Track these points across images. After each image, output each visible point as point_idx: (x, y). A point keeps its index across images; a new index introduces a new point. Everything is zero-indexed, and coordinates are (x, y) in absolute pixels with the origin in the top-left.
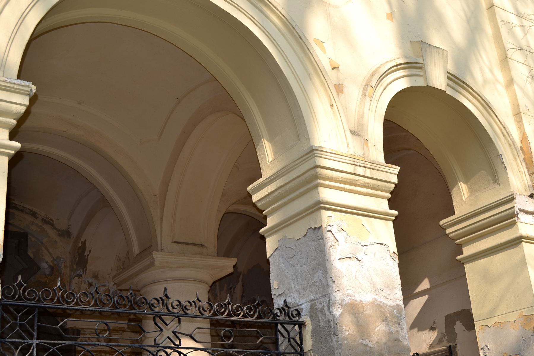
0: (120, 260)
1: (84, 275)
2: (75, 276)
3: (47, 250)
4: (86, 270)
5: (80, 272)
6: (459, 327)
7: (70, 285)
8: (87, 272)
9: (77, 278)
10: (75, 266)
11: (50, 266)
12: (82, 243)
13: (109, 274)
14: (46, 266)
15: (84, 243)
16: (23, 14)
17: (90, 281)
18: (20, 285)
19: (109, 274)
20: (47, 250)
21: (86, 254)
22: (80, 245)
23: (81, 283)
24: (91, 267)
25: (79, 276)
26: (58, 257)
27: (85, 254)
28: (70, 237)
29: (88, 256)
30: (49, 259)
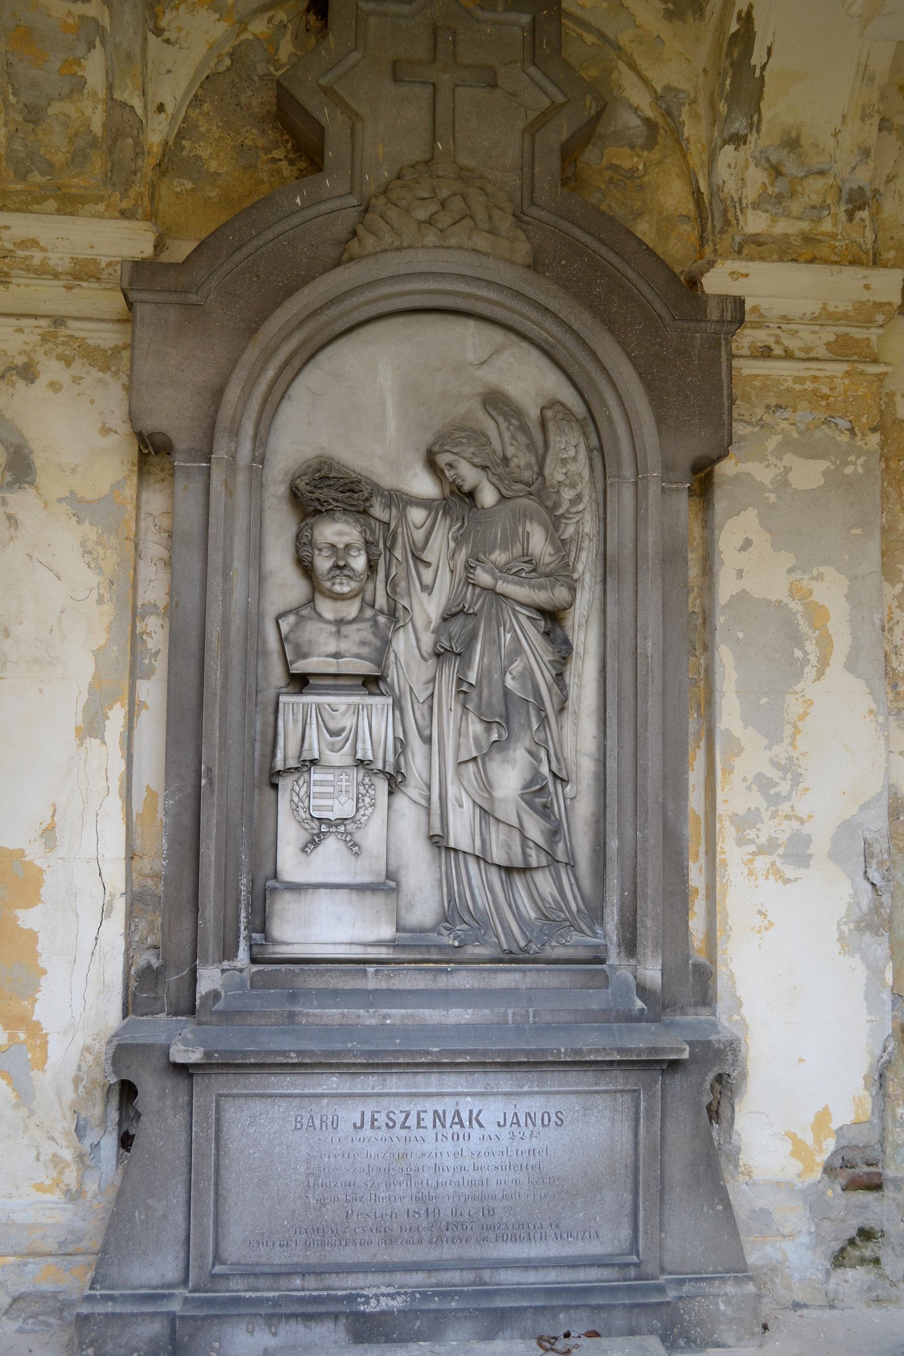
0: (871, 79)
1: (752, 138)
2: (726, 142)
3: (633, 67)
4: (760, 121)
5: (739, 125)
6: (502, 1123)
7: (710, 173)
8: (764, 127)
9: (729, 148)
10: (723, 107)
11: (647, 120)
12: (739, 18)
13: (835, 135)
14: (635, 122)
15: (747, 19)
16: (613, 384)
17: (774, 159)
18: (708, 1306)
19: (835, 135)
20: (633, 67)
21: (757, 58)
22: (734, 27)
23: (747, 167)
24: (777, 110)
25: (738, 140)
26: (668, 88)
27: (753, 61)
28: (702, 16)
29: (763, 68)
30: (639, 97)
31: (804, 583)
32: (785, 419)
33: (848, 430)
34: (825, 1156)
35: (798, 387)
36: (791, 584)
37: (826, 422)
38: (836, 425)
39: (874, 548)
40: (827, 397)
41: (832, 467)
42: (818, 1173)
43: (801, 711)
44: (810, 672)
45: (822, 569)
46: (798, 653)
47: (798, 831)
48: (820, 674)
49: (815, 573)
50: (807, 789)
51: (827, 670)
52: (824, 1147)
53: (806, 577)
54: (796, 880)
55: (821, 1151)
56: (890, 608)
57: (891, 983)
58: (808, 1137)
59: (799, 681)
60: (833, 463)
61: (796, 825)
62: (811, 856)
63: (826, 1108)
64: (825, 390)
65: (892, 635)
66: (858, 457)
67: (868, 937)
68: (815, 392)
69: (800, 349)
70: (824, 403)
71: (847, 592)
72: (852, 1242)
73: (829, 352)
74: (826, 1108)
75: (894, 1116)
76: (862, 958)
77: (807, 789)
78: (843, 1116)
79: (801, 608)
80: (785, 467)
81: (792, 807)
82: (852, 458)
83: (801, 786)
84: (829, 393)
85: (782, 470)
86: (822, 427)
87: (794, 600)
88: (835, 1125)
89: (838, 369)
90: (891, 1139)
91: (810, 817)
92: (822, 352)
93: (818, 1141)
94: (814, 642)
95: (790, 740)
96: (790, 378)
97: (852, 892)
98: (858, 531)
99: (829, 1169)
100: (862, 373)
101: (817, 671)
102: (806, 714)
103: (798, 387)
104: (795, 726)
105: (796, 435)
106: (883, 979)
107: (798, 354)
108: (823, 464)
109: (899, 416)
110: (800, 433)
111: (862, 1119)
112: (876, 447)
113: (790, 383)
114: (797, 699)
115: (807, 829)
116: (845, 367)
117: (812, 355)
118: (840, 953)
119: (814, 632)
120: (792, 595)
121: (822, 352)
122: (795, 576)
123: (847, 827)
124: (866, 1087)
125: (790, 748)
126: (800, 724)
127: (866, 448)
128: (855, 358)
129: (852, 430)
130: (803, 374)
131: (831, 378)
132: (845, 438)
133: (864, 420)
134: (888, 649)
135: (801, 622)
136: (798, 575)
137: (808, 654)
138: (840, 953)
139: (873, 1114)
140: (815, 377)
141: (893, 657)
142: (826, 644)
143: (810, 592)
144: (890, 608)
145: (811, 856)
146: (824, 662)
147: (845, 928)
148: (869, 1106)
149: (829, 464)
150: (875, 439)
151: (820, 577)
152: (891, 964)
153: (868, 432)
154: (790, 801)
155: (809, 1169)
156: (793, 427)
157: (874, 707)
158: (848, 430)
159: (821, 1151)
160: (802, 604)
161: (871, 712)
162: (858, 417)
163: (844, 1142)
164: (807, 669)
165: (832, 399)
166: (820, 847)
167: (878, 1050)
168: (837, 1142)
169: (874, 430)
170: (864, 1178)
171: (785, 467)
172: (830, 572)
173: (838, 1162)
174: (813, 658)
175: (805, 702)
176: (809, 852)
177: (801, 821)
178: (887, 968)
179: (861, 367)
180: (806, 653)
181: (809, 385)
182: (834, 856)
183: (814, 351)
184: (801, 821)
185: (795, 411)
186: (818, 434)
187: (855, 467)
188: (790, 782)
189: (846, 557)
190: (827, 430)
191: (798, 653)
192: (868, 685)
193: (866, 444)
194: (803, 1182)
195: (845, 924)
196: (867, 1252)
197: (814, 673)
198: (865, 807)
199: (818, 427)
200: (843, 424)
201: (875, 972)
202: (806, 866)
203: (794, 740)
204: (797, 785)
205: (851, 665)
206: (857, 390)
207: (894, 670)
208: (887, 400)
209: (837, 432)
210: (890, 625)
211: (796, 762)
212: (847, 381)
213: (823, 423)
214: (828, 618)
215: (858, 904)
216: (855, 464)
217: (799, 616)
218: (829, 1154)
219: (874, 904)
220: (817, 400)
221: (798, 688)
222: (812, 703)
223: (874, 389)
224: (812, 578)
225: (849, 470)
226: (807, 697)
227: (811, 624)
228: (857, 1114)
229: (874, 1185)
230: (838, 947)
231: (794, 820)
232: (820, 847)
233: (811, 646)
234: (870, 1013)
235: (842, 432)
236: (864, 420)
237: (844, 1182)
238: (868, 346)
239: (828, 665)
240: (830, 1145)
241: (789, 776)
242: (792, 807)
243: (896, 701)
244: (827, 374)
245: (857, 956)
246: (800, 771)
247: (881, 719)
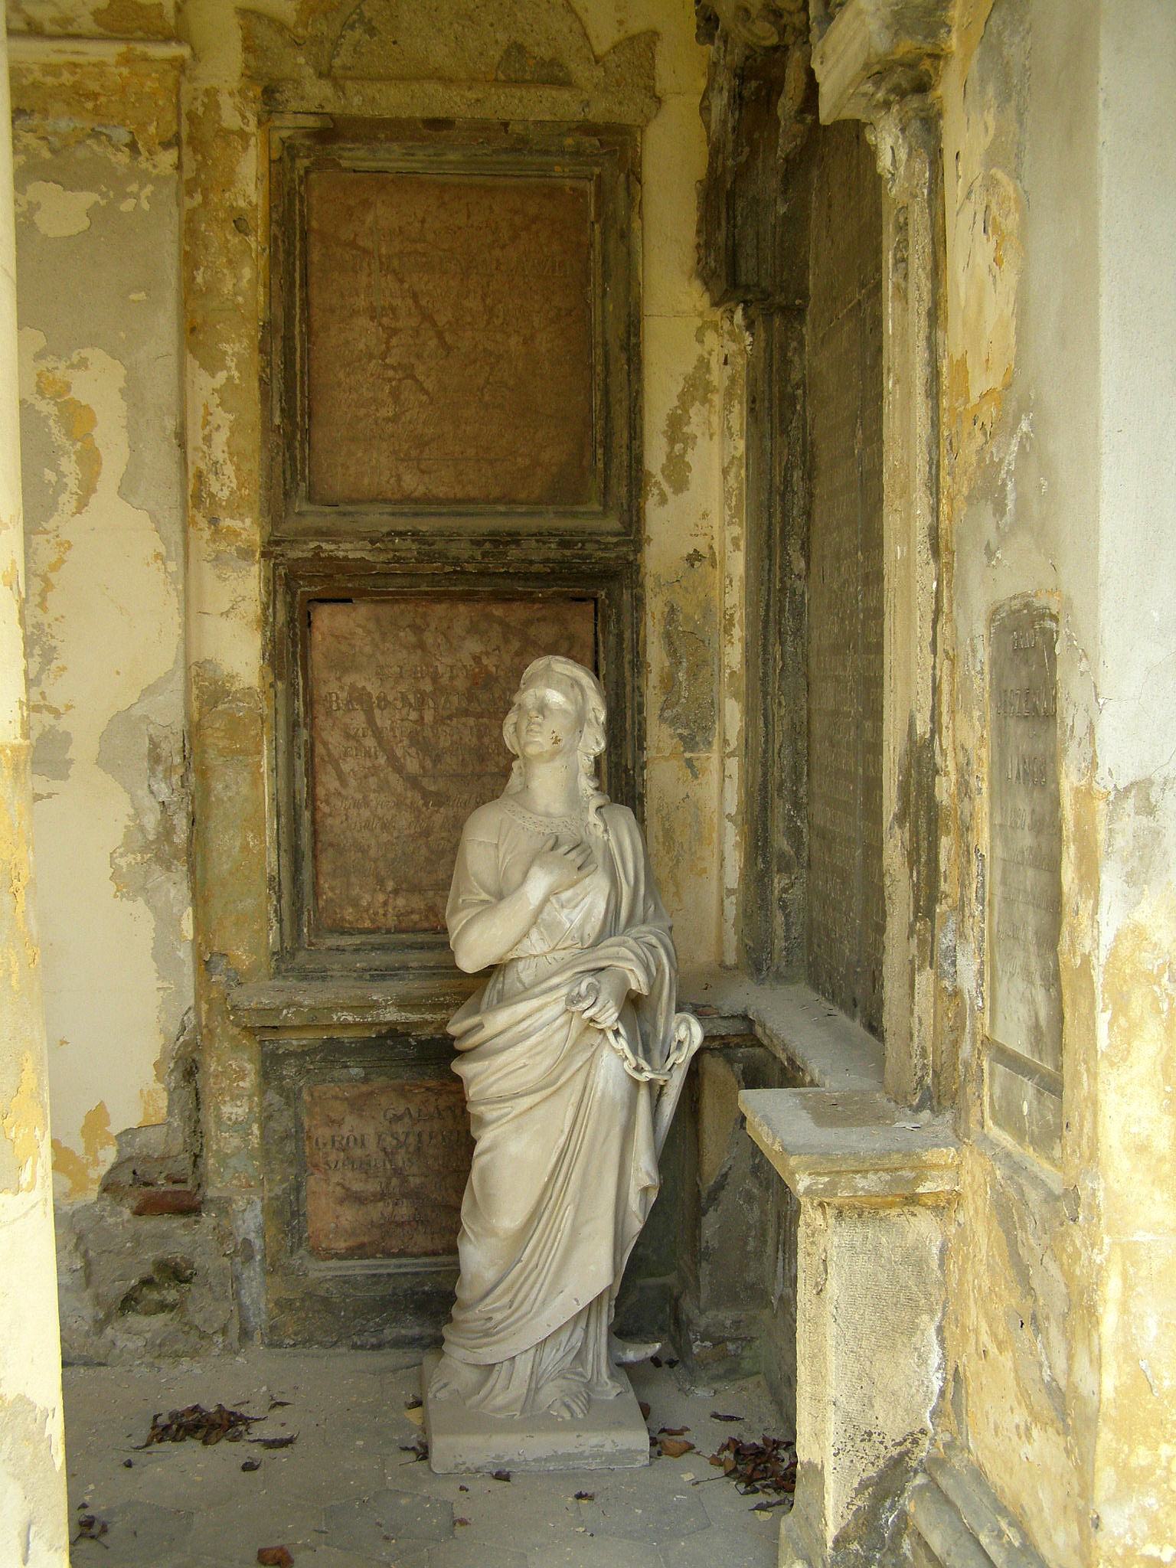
31: (58, 374)
32: (31, 131)
33: (126, 145)
34: (103, 1170)
35: (50, 80)
36: (39, 375)
37: (95, 134)
38: (109, 138)
39: (165, 324)
40: (95, 96)
41: (103, 203)
42: (93, 1194)
43: (54, 559)
44: (67, 502)
45: (86, 352)
46: (50, 475)
47: (52, 727)
48: (82, 504)
49: (75, 358)
50: (64, 669)
51: (93, 500)
52: (101, 1158)
53: (62, 365)
54: (49, 796)
55: (97, 1162)
56: (206, 407)
57: (190, 936)
58: (77, 1145)
59: (52, 515)
60: (103, 195)
61: (48, 718)
62: (71, 762)
63: (102, 1105)
64: (93, 86)
65: (210, 447)
66: (142, 187)
67: (158, 874)
68: (76, 88)
69: (54, 21)
70: (90, 105)
71: (122, 384)
72: (147, 1282)
73: (99, 25)
74: (102, 1105)
75: (219, 1117)
76: (147, 902)
77: (64, 669)
78: (126, 1115)
79: (54, 410)
80: (29, 203)
81: (43, 694)
82: (133, 188)
83: (53, 666)
84: (98, 89)
85: (25, 207)
86: (88, 142)
87: (44, 398)
88: (115, 1128)
89: (108, 52)
90: (215, 1147)
91: (69, 707)
92: (87, 24)
93: (90, 1148)
94: (74, 458)
95: (38, 599)
96: (36, 67)
97: (132, 812)
98: (141, 296)
99: (109, 1187)
100: (145, 59)
101: (79, 501)
102: (62, 561)
103: (50, 80)
104: (45, 579)
105: (47, 155)
106: (179, 932)
107: (49, 28)
108: (88, 198)
109: (224, 125)
110: (53, 151)
111: (154, 1121)
112: (170, 171)
113: (38, 75)
114: (48, 541)
115: (63, 725)
116: (121, 48)
117: (71, 30)
118: (115, 896)
119: (73, 445)
120: (41, 392)
121: (87, 24)
122: (43, 365)
123: (123, 721)
124: (159, 1078)
125: (39, 611)
126: (53, 577)
127: (155, 172)
128: (140, 34)
129: (133, 146)
130: (56, 59)
131: (100, 65)
132: (123, 158)
133: (152, 129)
134: (203, 467)
135: (55, 431)
136: (49, 362)
137: (65, 476)
138: (115, 896)
139: (170, 1113)
140: (75, 65)
141: (212, 477)
142: (90, 460)
143: (68, 387)
144: (206, 407)
145: (71, 762)
146: (88, 488)
147: (122, 862)
148: (163, 1102)
149: (99, 198)
150: (169, 157)
151: (83, 364)
152: (190, 910)
153: (159, 148)
154: (38, 685)
155: (80, 1187)
156: (42, 143)
157: (162, 550)
158: (126, 145)
159: (97, 1162)
160: (56, 404)
161: (158, 556)
162: (143, 126)
163: (129, 1151)
164: (64, 498)
165: (103, 99)
166: (84, 748)
167: (174, 1029)
168: (118, 1151)
169: (166, 145)
170: (169, 1198)
171: (29, 203)
172: (96, 356)
173: (126, 1178)
174: (72, 483)
175: (60, 544)
176: (68, 756)
177: (57, 713)
178: (185, 915)
179: (140, 48)
180: (61, 475)
181: (67, 78)
182: (106, 761)
183: (75, 25)
184: (57, 713)
185: (46, 117)
186: (81, 153)
187: (138, 200)
188: (38, 659)
189: (122, 335)
190: (95, 147)
191: (50, 475)
192: (153, 516)
193: (155, 166)
194: (72, 1204)
195: (122, 855)
196: (171, 1295)
197: (74, 503)
198: (149, 691)
199: (79, 142)
200: (122, 135)
201: (166, 922)
202: (65, 777)
203: (44, 599)
204: (50, 662)
205: (127, 490)
206: (142, 85)
207: (212, 496)
208: (206, 100)
209: (110, 149)
210: (206, 432)
211: (48, 630)
212: (125, 71)
213: (89, 136)
214: (93, 421)
215: (142, 829)
216: (137, 197)
217: (51, 422)
218: (108, 1167)
219: (164, 828)
220: (79, 101)
221: (50, 525)
222: (70, 546)
223: (170, 82)
224: (72, 366)
225: (127, 206)
226: (64, 537)
227: (69, 434)
228: (146, 1114)
229: (187, 1207)
230: (112, 887)
231: (45, 713)
232: (84, 748)
233: (69, 465)
234: (161, 977)
235: (118, 150)
236: (152, 129)
237: (135, 1204)
238: (161, 16)
239: (94, 491)
240: (109, 1155)
241: (37, 650)
242: (43, 694)
243: (214, 541)
244: (94, 59)
245: (140, 901)
246: (53, 642)
247: (172, 566)
